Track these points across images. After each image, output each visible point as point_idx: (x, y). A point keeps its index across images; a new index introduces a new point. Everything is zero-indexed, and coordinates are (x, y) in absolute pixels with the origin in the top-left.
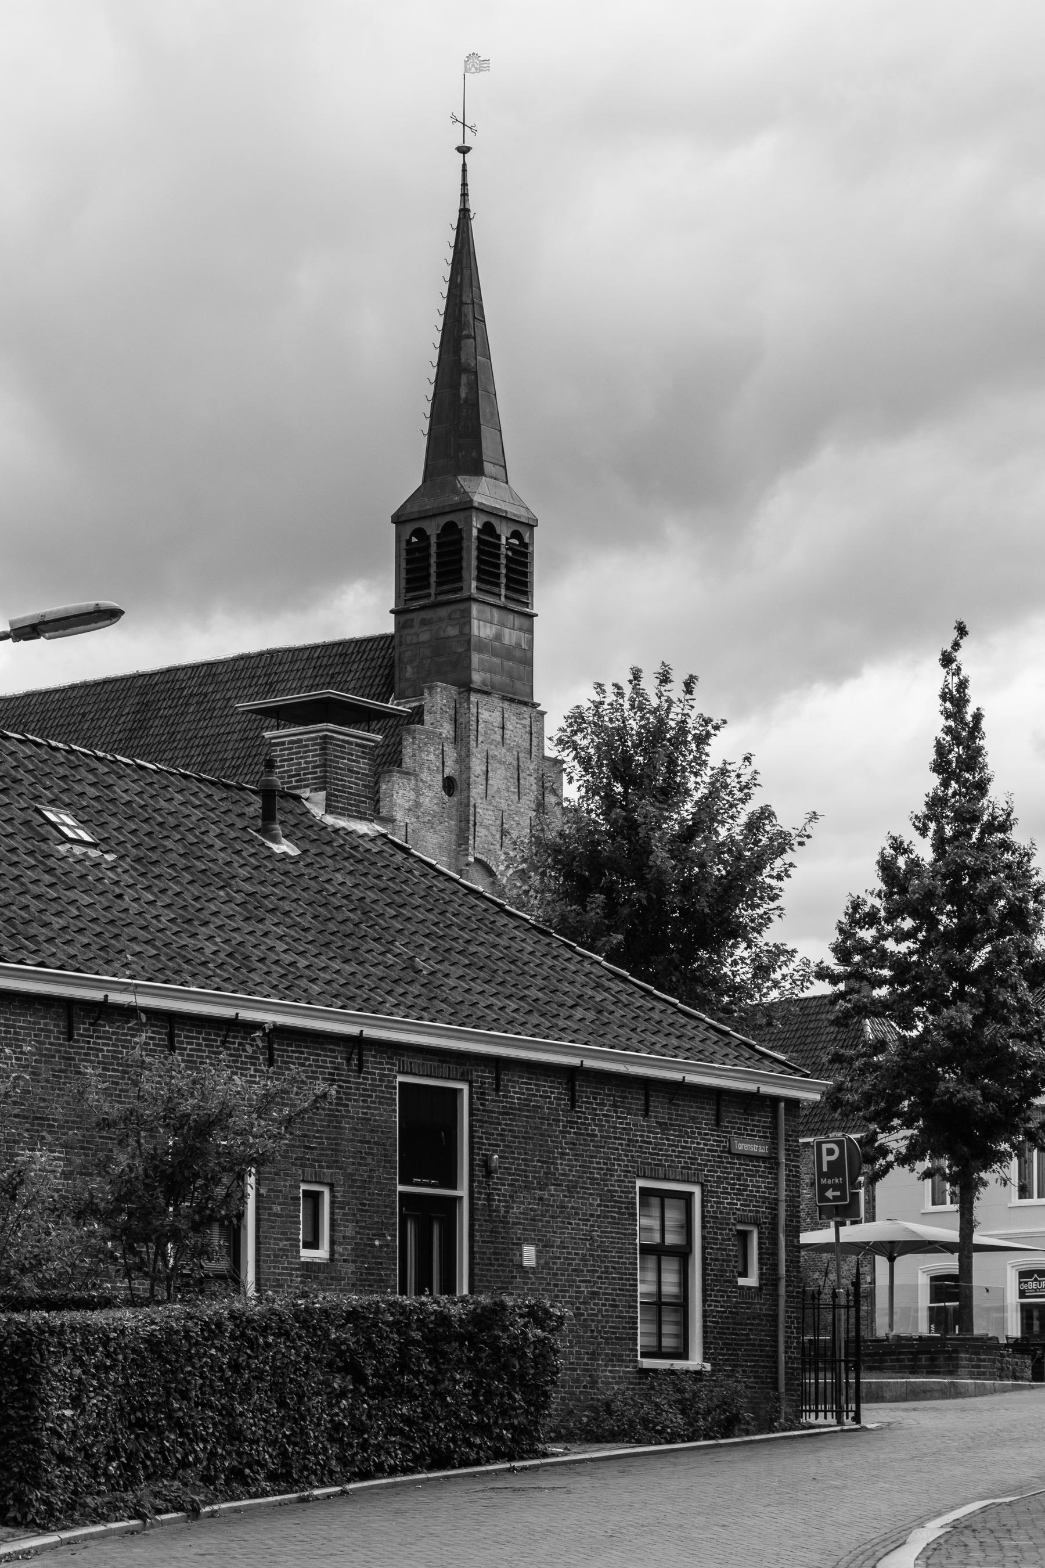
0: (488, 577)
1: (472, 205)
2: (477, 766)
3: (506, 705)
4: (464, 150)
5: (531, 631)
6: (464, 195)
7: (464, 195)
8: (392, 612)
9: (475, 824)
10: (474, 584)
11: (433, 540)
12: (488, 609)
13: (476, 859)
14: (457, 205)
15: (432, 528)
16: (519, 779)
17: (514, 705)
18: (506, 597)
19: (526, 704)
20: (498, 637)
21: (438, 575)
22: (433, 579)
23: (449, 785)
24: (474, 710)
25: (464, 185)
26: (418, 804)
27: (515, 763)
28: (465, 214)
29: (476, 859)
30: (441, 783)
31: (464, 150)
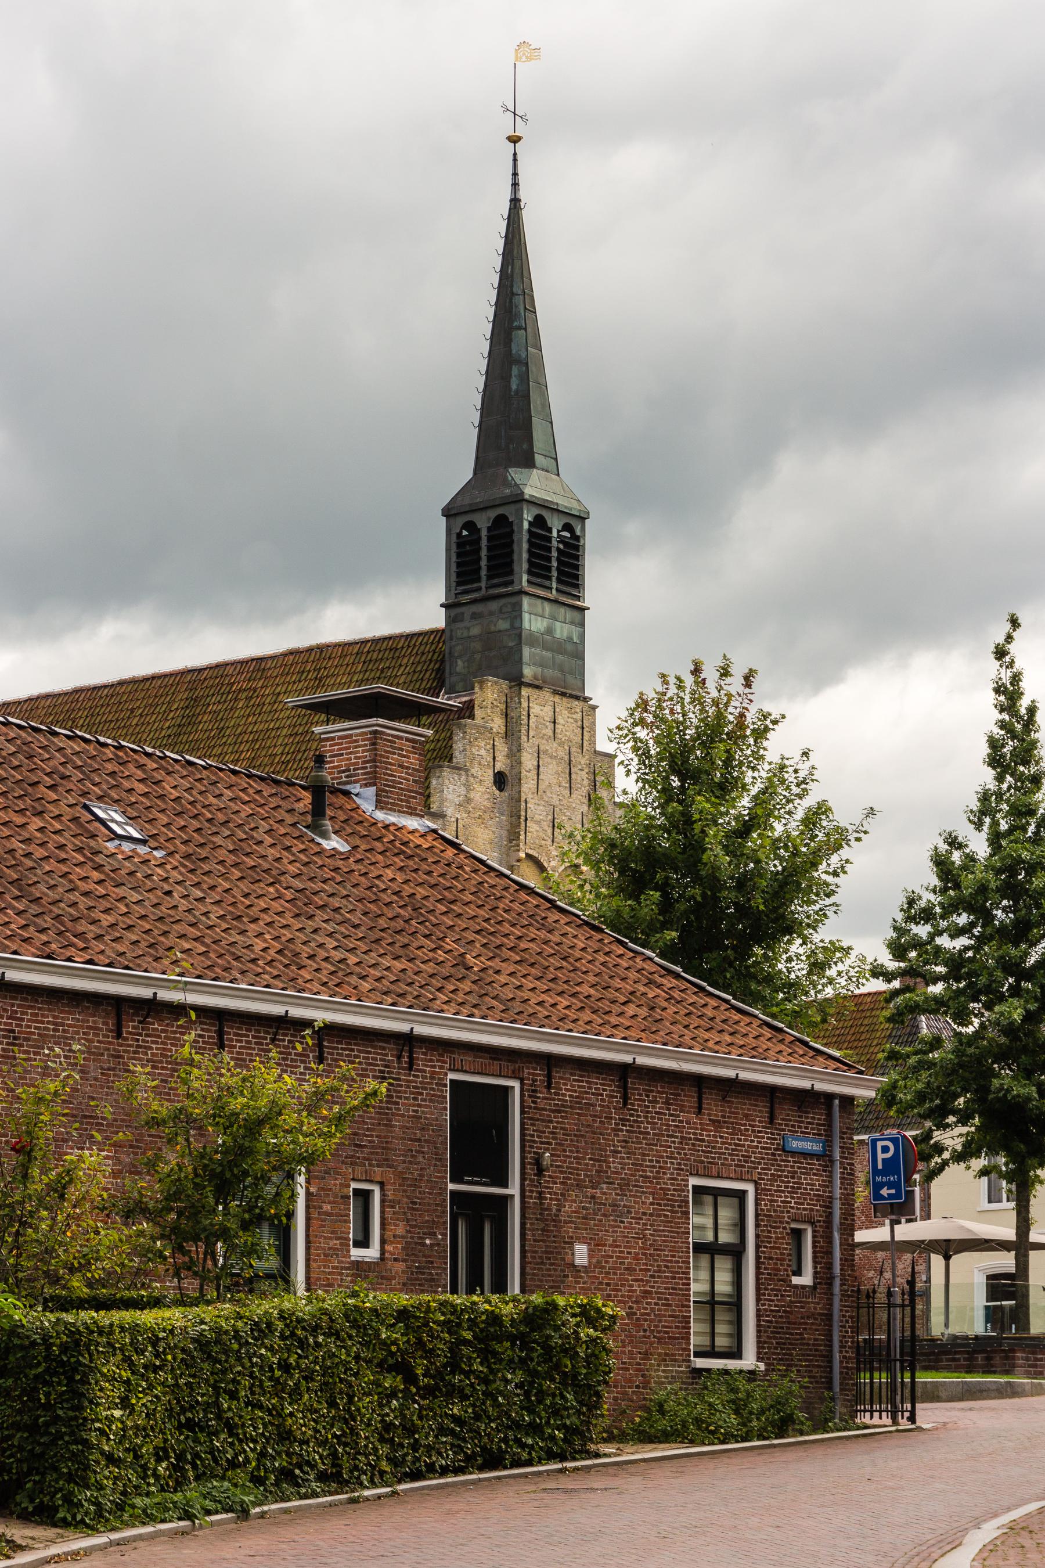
0: (539, 571)
1: (522, 195)
2: (528, 761)
3: (557, 699)
4: (514, 140)
5: (582, 624)
6: (515, 185)
7: (515, 185)
8: (442, 606)
9: (526, 819)
10: (525, 577)
11: (484, 533)
12: (539, 602)
13: (527, 855)
14: (508, 195)
15: (483, 522)
16: (570, 774)
17: (565, 699)
18: (557, 590)
19: (577, 698)
20: (550, 631)
21: (489, 568)
22: (484, 572)
23: (500, 780)
24: (525, 704)
25: (515, 174)
26: (468, 800)
27: (567, 758)
28: (515, 203)
29: (527, 855)
30: (491, 778)
31: (514, 140)
